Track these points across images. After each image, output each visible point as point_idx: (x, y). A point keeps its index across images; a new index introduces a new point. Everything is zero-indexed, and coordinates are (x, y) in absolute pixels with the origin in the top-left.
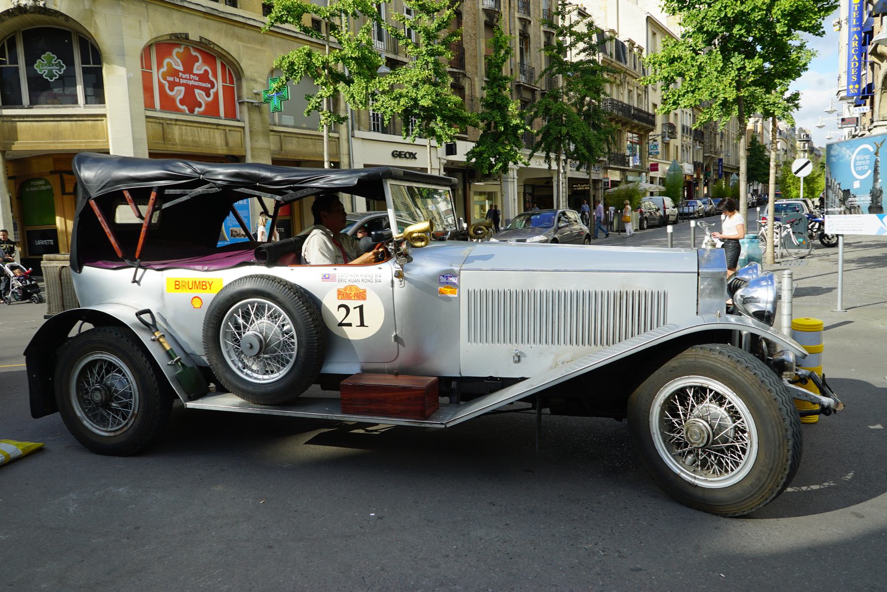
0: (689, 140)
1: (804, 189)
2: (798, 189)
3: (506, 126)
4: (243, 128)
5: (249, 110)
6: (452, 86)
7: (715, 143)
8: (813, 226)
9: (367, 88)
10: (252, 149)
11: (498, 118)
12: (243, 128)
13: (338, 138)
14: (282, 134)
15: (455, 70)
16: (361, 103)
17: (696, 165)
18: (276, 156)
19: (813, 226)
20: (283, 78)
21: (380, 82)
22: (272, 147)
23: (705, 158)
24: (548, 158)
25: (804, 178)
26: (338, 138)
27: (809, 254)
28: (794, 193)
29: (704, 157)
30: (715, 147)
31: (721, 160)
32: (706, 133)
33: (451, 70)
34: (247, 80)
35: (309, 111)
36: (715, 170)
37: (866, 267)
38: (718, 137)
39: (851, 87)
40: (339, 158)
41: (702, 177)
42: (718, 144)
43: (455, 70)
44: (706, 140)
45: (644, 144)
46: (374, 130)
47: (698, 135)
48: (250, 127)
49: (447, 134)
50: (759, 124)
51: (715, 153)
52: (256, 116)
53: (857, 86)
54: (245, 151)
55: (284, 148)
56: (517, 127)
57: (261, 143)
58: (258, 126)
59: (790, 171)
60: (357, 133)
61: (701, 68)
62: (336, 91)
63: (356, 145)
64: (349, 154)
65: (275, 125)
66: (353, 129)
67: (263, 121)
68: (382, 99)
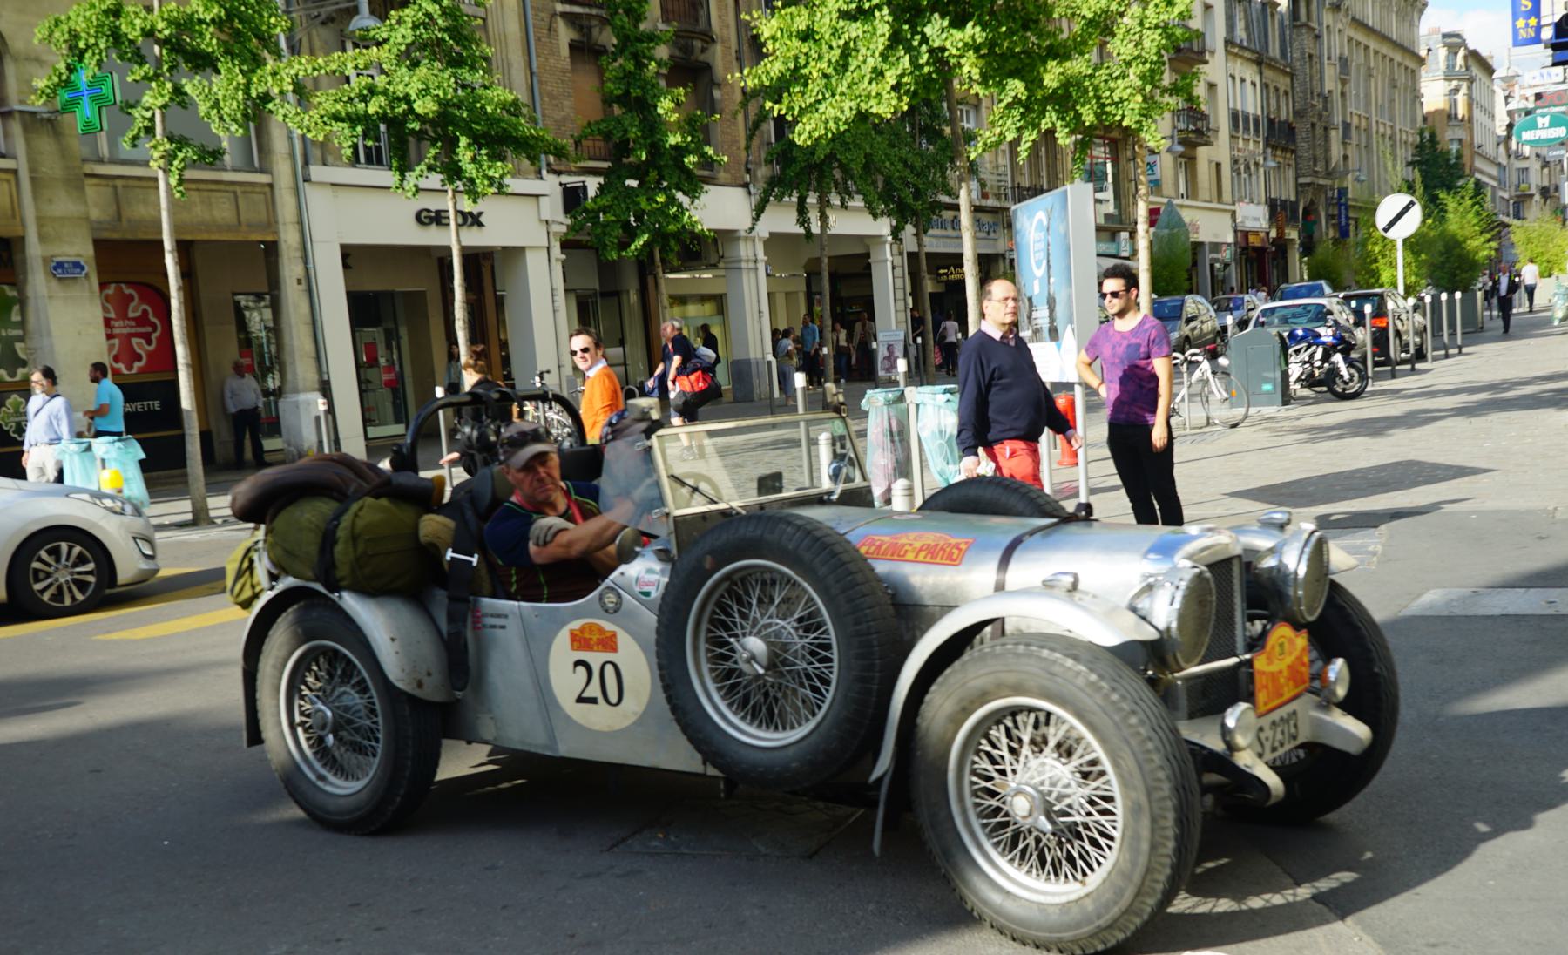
0: (1254, 147)
1: (1407, 265)
2: (1393, 265)
3: (656, 149)
4: (15, 172)
5: (26, 129)
6: (574, 47)
7: (1327, 150)
8: (1312, 356)
9: (248, 84)
10: (41, 221)
11: (634, 132)
12: (15, 172)
13: (271, 186)
14: (119, 183)
15: (577, 9)
16: (235, 120)
17: (1277, 209)
18: (106, 235)
19: (1312, 356)
20: (62, 67)
21: (274, 74)
22: (95, 214)
23: (1300, 188)
24: (802, 210)
25: (1405, 241)
26: (271, 186)
27: (1246, 416)
28: (1385, 276)
29: (1298, 185)
30: (1327, 161)
31: (1343, 192)
32: (1301, 128)
33: (568, 8)
34: (16, 60)
35: (135, 138)
36: (1330, 217)
37: (1330, 438)
38: (1335, 136)
39: (1521, 23)
40: (276, 232)
41: (1293, 234)
42: (1336, 151)
43: (577, 9)
44: (1302, 145)
45: (1123, 162)
46: (369, 161)
47: (1279, 135)
48: (32, 170)
49: (486, 176)
50: (1461, 98)
51: (1329, 174)
52: (45, 144)
53: (1533, 22)
54: (23, 225)
55: (126, 213)
56: (680, 151)
57: (63, 205)
58: (51, 166)
59: (1374, 225)
60: (316, 172)
61: (846, 53)
62: (178, 91)
63: (318, 203)
64: (301, 223)
65: (101, 161)
66: (306, 163)
67: (64, 153)
68: (282, 111)
